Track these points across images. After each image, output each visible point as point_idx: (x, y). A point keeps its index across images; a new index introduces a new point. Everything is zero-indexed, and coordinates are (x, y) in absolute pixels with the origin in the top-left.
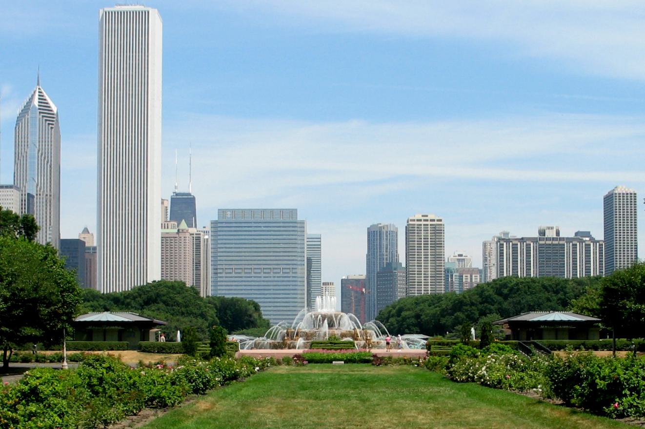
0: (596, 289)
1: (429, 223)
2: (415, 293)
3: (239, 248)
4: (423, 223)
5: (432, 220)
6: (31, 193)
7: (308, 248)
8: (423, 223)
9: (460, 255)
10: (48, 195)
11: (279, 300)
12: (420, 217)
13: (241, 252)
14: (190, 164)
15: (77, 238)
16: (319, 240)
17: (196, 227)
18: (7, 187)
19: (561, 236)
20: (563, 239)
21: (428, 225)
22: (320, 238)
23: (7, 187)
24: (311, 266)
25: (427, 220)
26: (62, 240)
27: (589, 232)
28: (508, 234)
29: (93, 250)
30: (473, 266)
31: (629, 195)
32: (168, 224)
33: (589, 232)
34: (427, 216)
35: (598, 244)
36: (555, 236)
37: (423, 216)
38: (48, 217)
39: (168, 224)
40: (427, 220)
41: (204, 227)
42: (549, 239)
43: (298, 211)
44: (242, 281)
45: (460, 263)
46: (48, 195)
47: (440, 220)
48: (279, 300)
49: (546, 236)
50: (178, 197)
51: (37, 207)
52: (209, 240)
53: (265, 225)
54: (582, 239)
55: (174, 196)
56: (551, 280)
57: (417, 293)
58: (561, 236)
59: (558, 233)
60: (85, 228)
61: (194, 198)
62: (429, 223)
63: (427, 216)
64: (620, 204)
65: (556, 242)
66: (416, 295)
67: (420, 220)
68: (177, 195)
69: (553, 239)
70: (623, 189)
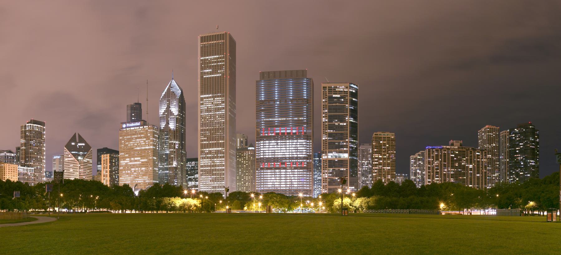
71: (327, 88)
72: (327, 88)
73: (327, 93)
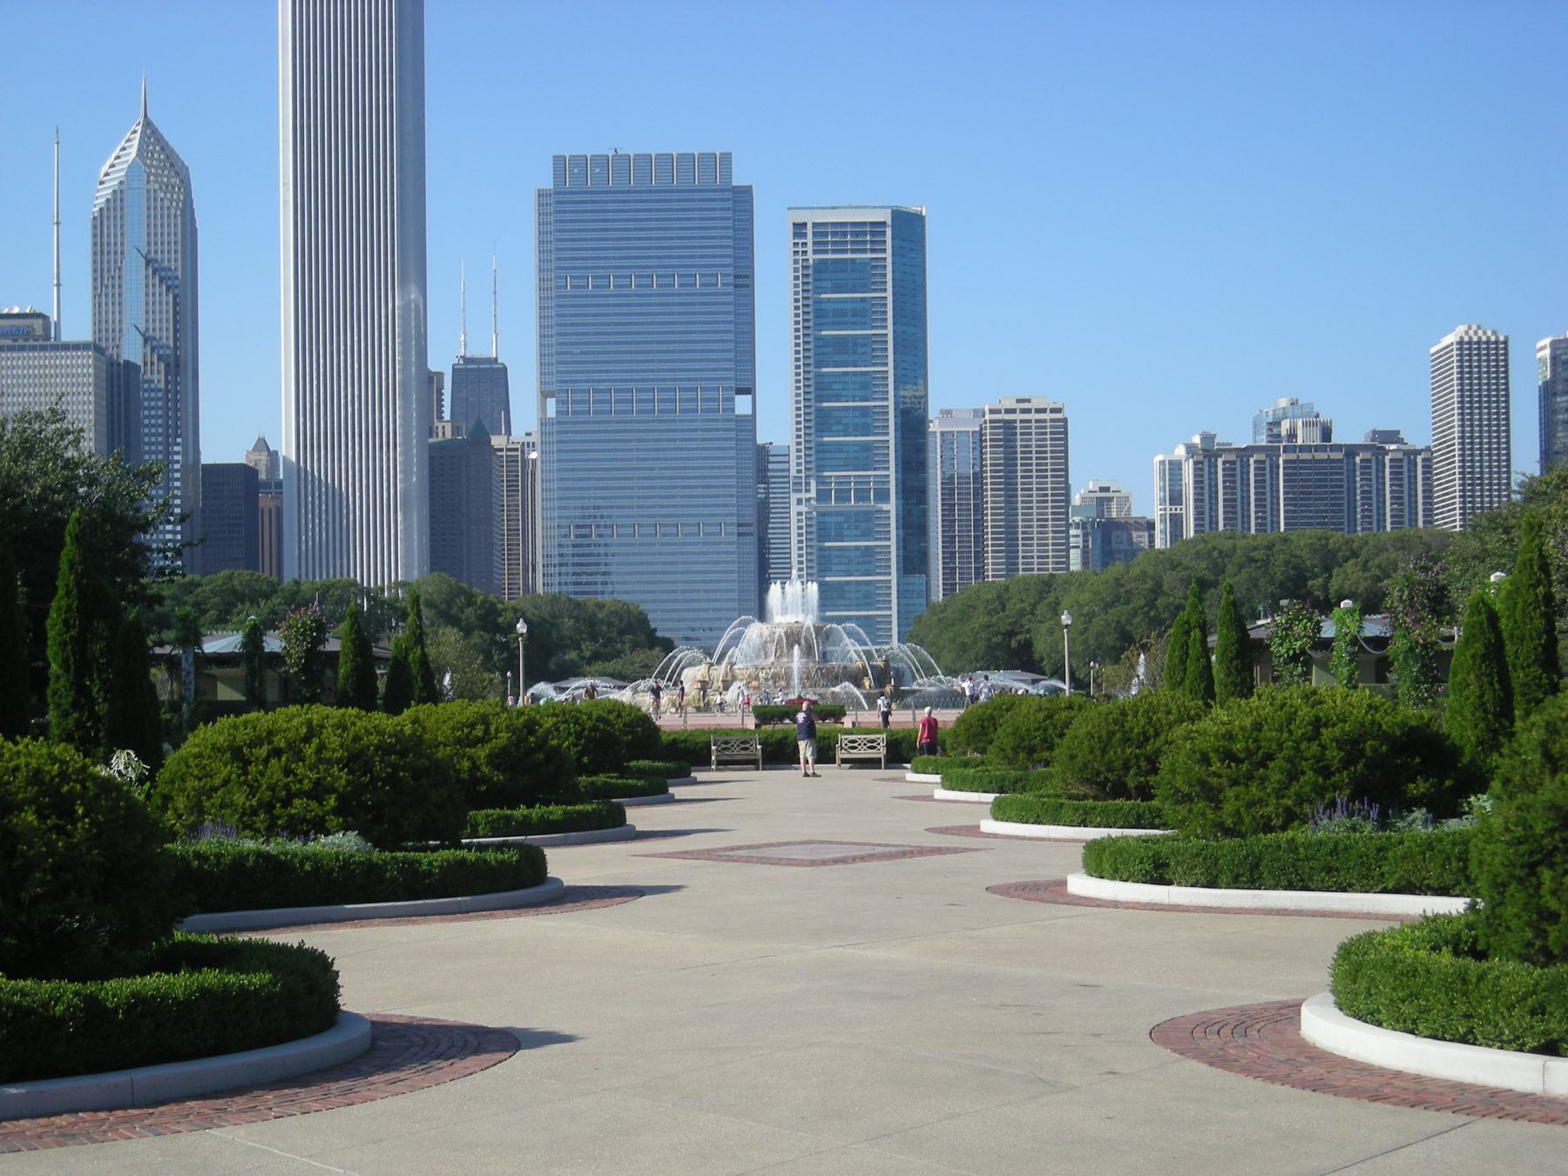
0: (656, 692)
1: (1033, 416)
2: (1033, 570)
3: (625, 431)
5: (1038, 411)
9: (1103, 489)
10: (172, 365)
12: (1011, 404)
14: (495, 293)
15: (243, 461)
16: (786, 459)
17: (509, 432)
19: (1336, 439)
20: (1338, 448)
21: (1030, 421)
22: (788, 455)
24: (768, 518)
25: (1028, 411)
27: (1398, 432)
28: (1213, 437)
29: (276, 488)
30: (1134, 514)
32: (443, 427)
33: (1398, 432)
34: (1029, 401)
37: (1018, 401)
38: (338, 565)
39: (443, 427)
40: (1028, 411)
41: (528, 434)
42: (1303, 448)
44: (675, 449)
46: (172, 365)
47: (1059, 410)
50: (469, 367)
52: (539, 464)
54: (1384, 448)
55: (458, 364)
56: (1106, 583)
57: (1039, 570)
58: (1336, 439)
59: (1326, 433)
60: (259, 439)
61: (505, 369)
62: (1033, 416)
63: (1029, 401)
64: (1488, 361)
65: (1323, 456)
66: (1036, 572)
67: (1013, 411)
69: (1317, 448)
70: (1471, 333)
71: (810, 226)
72: (810, 226)
73: (810, 248)
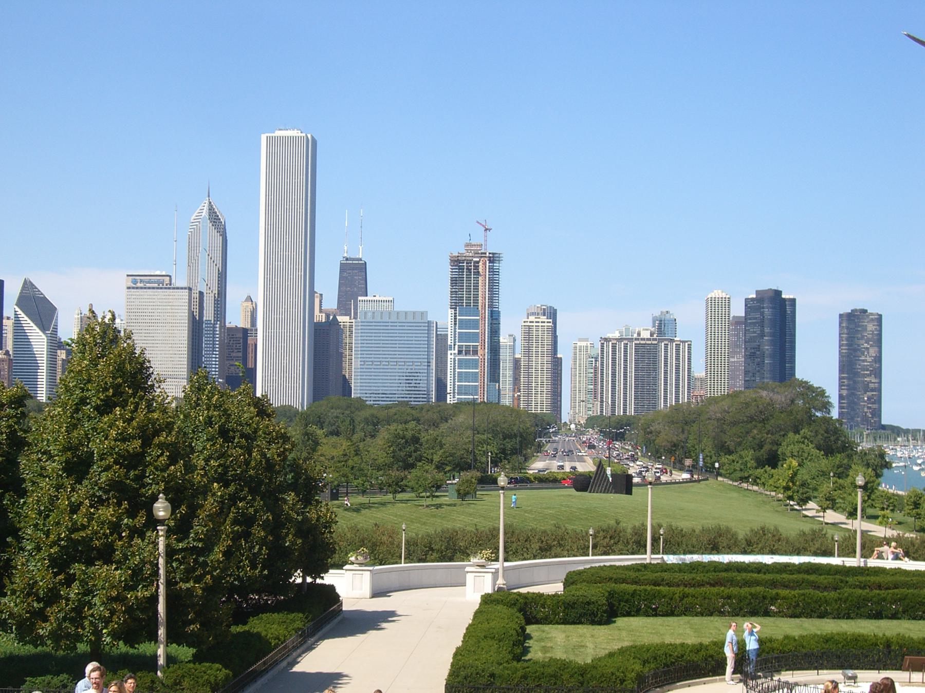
1: (540, 324)
4: (534, 324)
6: (202, 291)
7: (461, 377)
8: (534, 324)
11: (388, 346)
13: (382, 376)
18: (182, 288)
23: (182, 288)
25: (539, 322)
26: (230, 329)
31: (724, 299)
35: (686, 344)
36: (649, 337)
43: (630, 496)
45: (837, 501)
48: (388, 346)
49: (642, 337)
51: (206, 303)
53: (400, 324)
62: (540, 324)
68: (347, 259)
69: (648, 339)
